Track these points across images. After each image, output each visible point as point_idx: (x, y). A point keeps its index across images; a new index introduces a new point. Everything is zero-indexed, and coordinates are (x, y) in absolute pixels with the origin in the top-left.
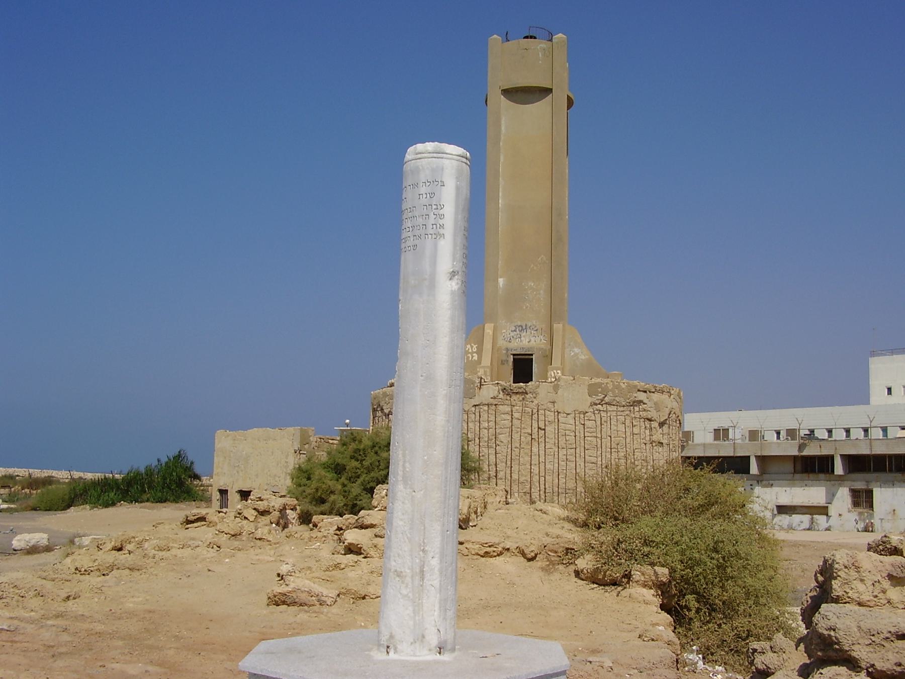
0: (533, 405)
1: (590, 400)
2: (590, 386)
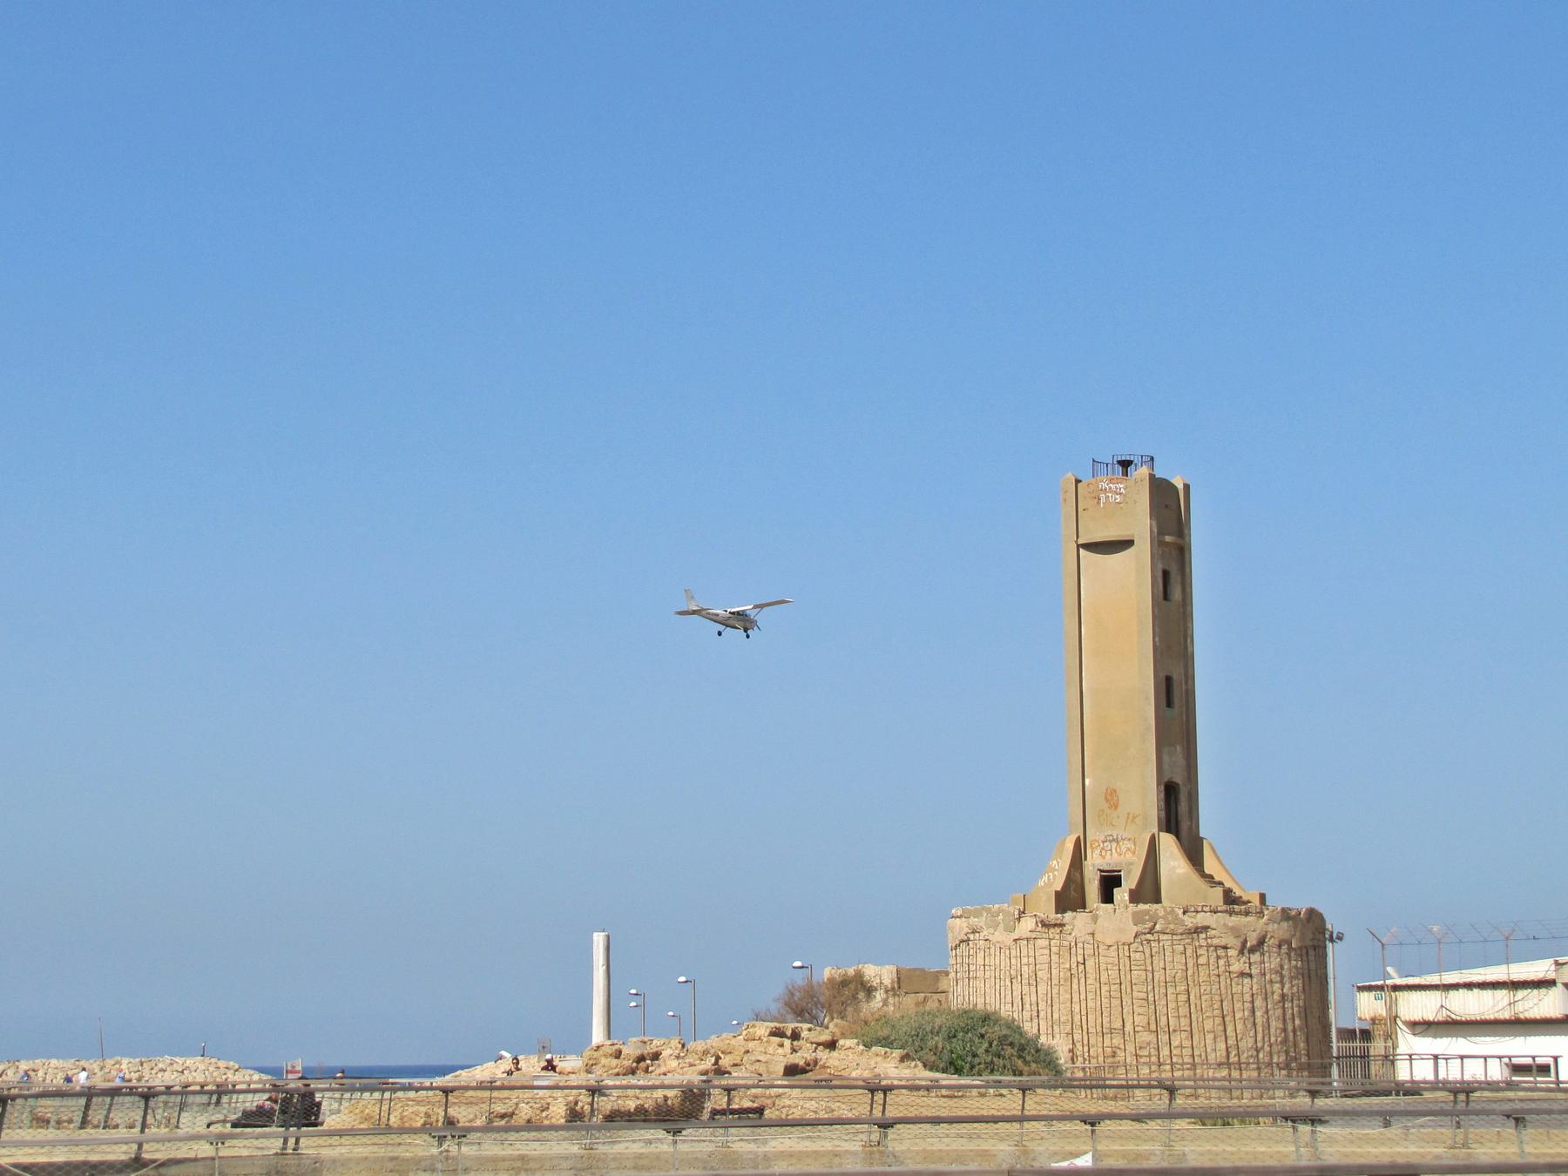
0: (1070, 938)
1: (1135, 929)
2: (1135, 914)
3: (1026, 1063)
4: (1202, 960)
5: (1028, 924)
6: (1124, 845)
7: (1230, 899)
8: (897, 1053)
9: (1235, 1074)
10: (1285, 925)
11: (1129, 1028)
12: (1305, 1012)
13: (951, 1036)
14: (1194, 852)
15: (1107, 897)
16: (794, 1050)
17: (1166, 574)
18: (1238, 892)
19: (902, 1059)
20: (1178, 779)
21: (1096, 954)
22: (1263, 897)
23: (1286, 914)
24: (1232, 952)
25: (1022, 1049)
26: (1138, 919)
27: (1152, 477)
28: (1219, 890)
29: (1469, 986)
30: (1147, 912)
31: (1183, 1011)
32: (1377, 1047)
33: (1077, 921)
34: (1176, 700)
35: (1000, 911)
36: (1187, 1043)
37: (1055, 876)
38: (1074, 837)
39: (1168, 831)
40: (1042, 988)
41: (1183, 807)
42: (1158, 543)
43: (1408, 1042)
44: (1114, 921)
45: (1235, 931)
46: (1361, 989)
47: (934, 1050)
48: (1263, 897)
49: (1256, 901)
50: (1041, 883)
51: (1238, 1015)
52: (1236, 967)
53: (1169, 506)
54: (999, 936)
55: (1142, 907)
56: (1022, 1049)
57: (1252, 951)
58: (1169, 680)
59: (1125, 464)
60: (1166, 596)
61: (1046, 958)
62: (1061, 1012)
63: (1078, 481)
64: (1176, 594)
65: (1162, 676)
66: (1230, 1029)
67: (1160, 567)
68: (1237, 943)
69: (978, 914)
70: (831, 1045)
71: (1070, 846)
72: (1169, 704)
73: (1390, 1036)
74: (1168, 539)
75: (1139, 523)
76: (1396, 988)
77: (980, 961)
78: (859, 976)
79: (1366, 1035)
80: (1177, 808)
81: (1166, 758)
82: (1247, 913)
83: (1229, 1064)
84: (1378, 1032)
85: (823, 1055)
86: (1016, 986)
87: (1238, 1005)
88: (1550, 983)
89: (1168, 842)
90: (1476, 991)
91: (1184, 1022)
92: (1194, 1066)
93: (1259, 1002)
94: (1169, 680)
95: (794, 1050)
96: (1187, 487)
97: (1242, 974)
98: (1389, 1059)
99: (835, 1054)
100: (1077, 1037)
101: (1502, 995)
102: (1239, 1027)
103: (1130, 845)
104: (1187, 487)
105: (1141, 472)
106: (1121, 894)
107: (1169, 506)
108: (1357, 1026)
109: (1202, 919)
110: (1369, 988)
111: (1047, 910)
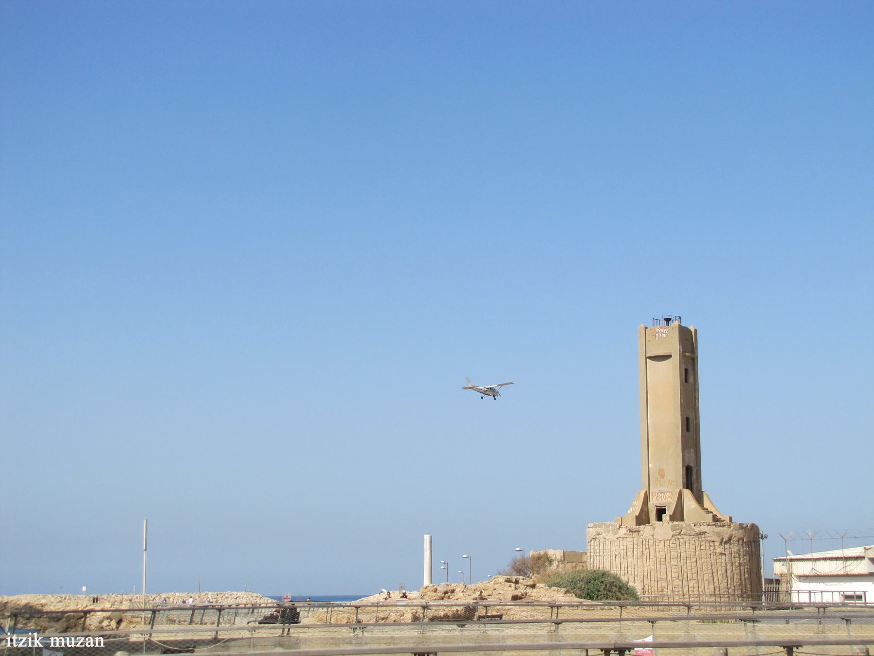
2: (672, 526)
3: (623, 594)
4: (703, 547)
5: (623, 531)
6: (667, 495)
7: (716, 519)
8: (563, 590)
9: (718, 599)
10: (741, 531)
11: (669, 578)
12: (750, 571)
13: (588, 582)
14: (699, 498)
15: (660, 519)
16: (516, 589)
17: (686, 371)
18: (719, 516)
19: (566, 593)
20: (692, 465)
21: (654, 544)
22: (731, 518)
23: (741, 527)
24: (716, 544)
25: (620, 588)
26: (673, 528)
27: (680, 326)
28: (711, 515)
29: (825, 559)
30: (677, 525)
31: (694, 570)
32: (783, 587)
33: (645, 529)
34: (691, 428)
35: (610, 525)
36: (696, 585)
37: (636, 509)
38: (644, 491)
39: (687, 488)
40: (630, 560)
41: (694, 477)
42: (683, 356)
43: (797, 585)
44: (663, 529)
45: (718, 534)
46: (775, 560)
47: (580, 589)
48: (731, 518)
49: (728, 520)
50: (629, 512)
51: (719, 572)
52: (718, 550)
53: (688, 341)
54: (610, 536)
55: (675, 523)
56: (620, 588)
57: (726, 543)
58: (687, 419)
59: (668, 320)
60: (686, 381)
61: (631, 547)
62: (638, 571)
63: (646, 328)
64: (691, 379)
65: (685, 417)
66: (715, 579)
67: (684, 367)
68: (718, 539)
69: (600, 526)
70: (533, 586)
71: (642, 495)
72: (688, 430)
73: (789, 582)
74: (687, 354)
75: (674, 347)
76: (791, 560)
77: (601, 548)
78: (546, 554)
79: (778, 582)
80: (691, 477)
81: (686, 455)
82: (723, 526)
83: (715, 595)
84: (783, 580)
85: (529, 591)
86: (618, 559)
87: (719, 568)
88: (863, 558)
89: (687, 493)
90: (828, 561)
91: (695, 576)
92: (699, 596)
93: (729, 567)
94: (687, 419)
95: (516, 589)
96: (696, 331)
97: (721, 554)
98: (789, 593)
99: (535, 590)
100: (646, 582)
101: (840, 563)
102: (720, 578)
103: (670, 494)
104: (696, 331)
105: (675, 324)
106: (666, 517)
107: (688, 341)
108: (774, 578)
109: (703, 528)
110: (779, 560)
111: (632, 524)
